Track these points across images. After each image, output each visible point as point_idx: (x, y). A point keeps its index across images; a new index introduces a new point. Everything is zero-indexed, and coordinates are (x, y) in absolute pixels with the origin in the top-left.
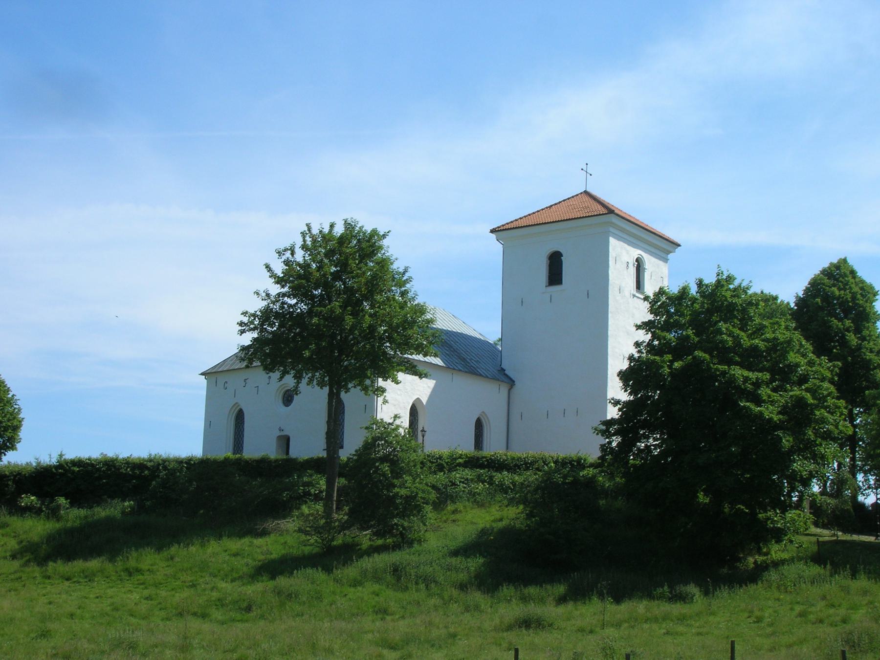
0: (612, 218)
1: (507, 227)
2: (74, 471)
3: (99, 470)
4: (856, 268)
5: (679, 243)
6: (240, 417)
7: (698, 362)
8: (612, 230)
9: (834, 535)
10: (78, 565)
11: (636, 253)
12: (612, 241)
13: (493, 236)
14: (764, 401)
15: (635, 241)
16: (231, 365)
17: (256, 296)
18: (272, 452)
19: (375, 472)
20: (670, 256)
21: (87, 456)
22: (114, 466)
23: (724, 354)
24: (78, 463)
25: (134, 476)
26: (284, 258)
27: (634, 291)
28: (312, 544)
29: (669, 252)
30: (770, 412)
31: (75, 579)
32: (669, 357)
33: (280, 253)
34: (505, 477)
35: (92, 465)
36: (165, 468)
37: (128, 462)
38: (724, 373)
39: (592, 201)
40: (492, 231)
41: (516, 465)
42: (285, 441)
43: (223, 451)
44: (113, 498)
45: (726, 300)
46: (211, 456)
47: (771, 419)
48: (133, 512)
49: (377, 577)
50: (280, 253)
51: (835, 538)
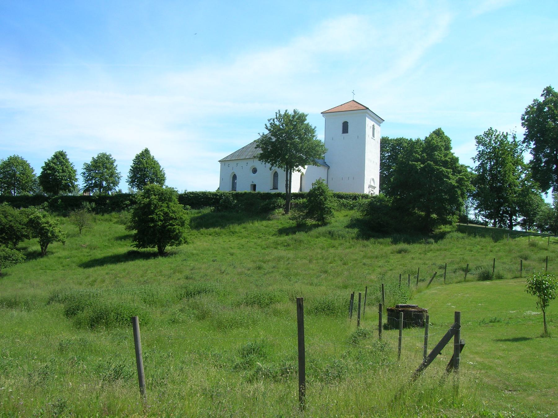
0: (367, 111)
1: (326, 112)
2: (191, 196)
3: (200, 196)
4: (444, 131)
5: (384, 120)
6: (234, 177)
7: (429, 165)
8: (367, 115)
9: (200, 212)
10: (211, 230)
11: (373, 123)
12: (367, 118)
13: (322, 115)
14: (451, 179)
15: (372, 119)
16: (231, 158)
17: (259, 134)
18: (248, 190)
19: (318, 199)
20: (381, 124)
21: (195, 191)
22: (205, 194)
23: (436, 162)
24: (192, 193)
25: (212, 199)
26: (270, 122)
27: (372, 137)
28: (293, 223)
29: (381, 123)
30: (454, 183)
31: (213, 235)
32: (419, 163)
33: (269, 120)
34: (344, 201)
35: (198, 194)
36: (224, 196)
37: (200, 193)
38: (438, 169)
39: (358, 104)
40: (321, 113)
41: (347, 197)
42: (254, 187)
43: (227, 190)
44: (206, 206)
45: (435, 144)
46: (221, 191)
47: (454, 185)
48: (214, 211)
49: (324, 235)
50: (269, 120)
51: (200, 214)
